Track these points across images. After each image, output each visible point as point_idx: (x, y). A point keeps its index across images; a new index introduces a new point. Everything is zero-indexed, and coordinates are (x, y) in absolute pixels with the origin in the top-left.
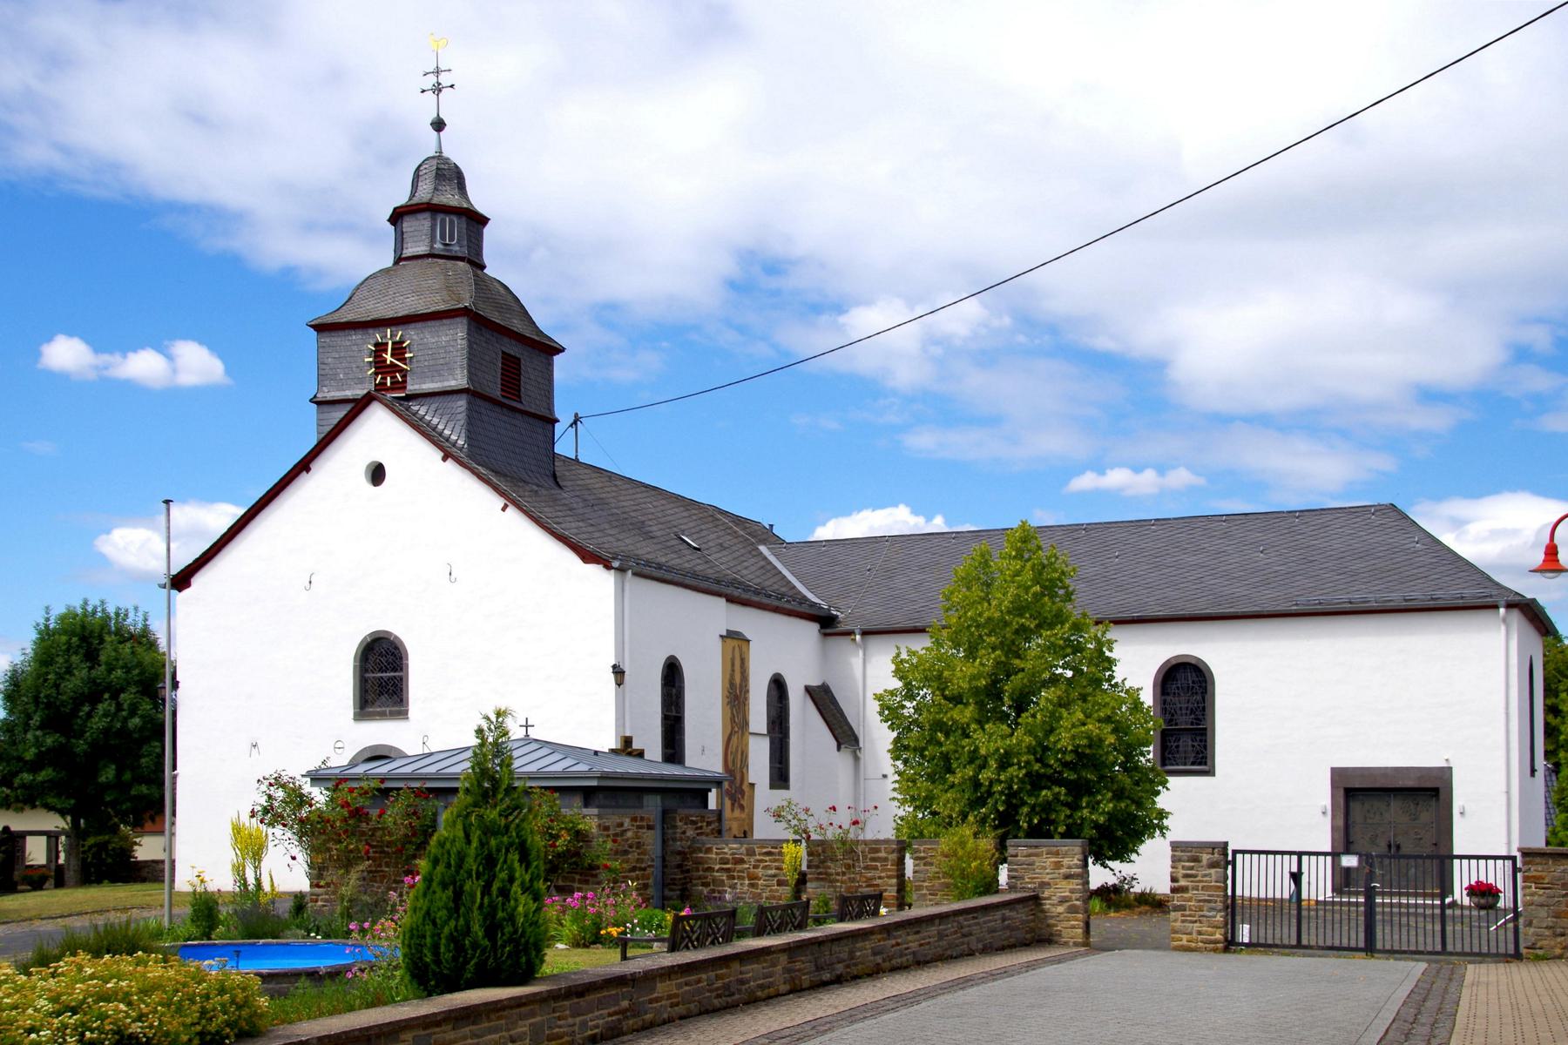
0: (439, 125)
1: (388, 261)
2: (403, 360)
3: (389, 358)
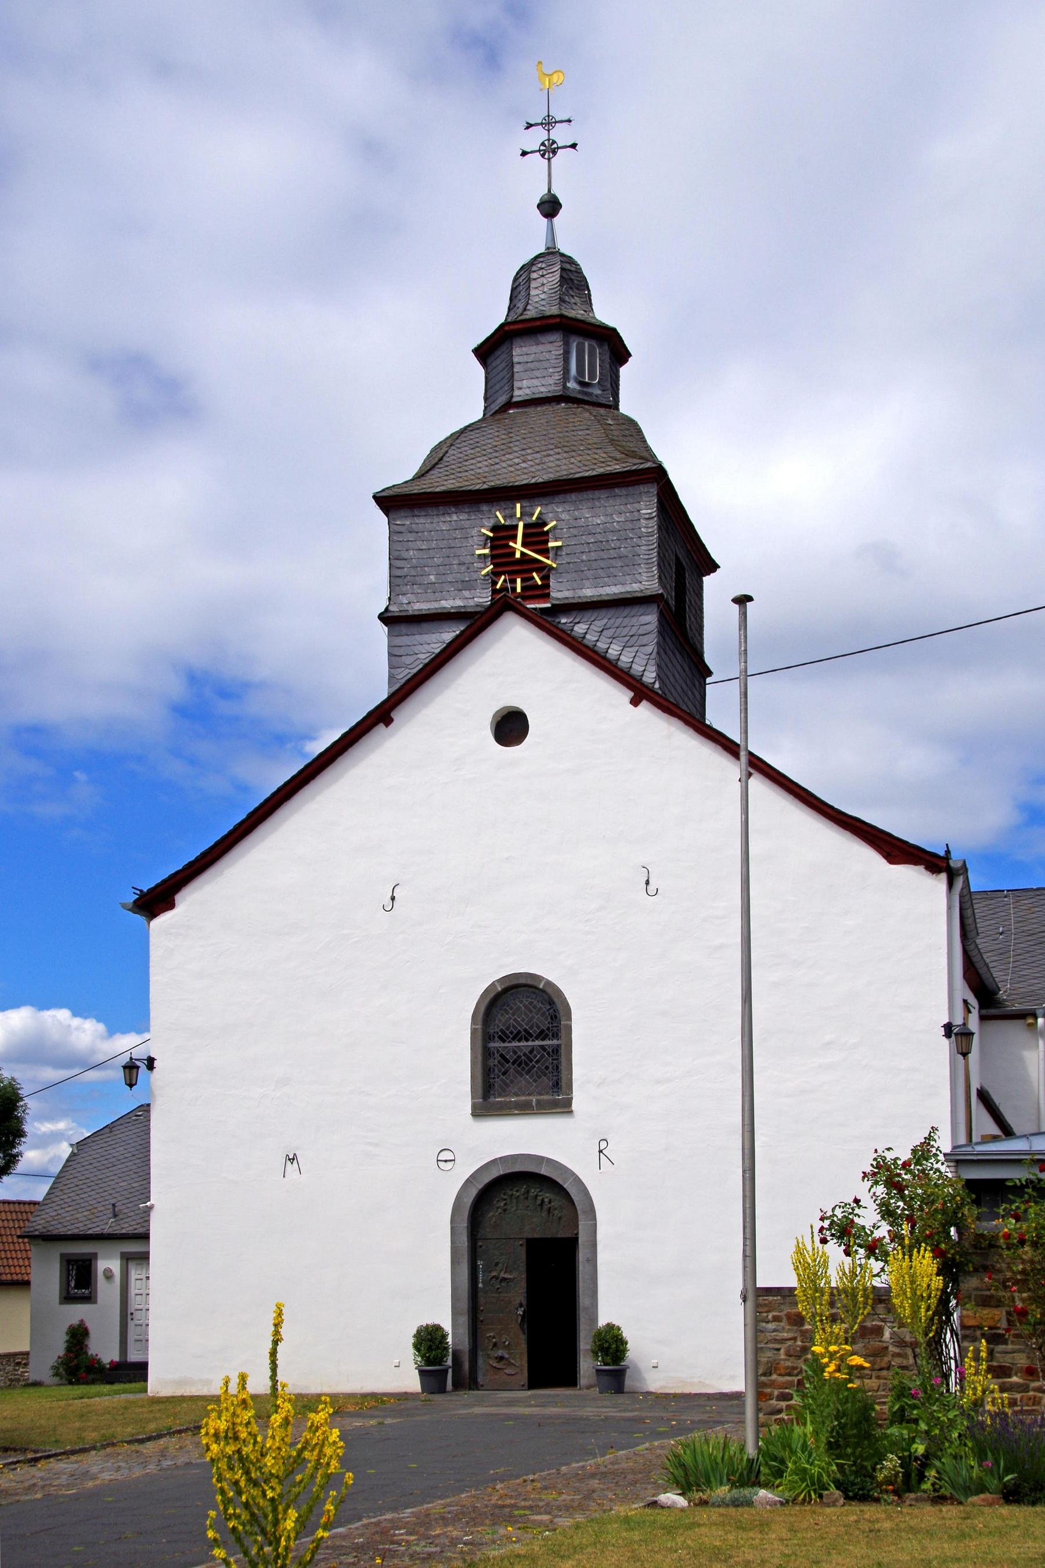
0: (550, 207)
1: (475, 411)
2: (545, 552)
3: (518, 546)
